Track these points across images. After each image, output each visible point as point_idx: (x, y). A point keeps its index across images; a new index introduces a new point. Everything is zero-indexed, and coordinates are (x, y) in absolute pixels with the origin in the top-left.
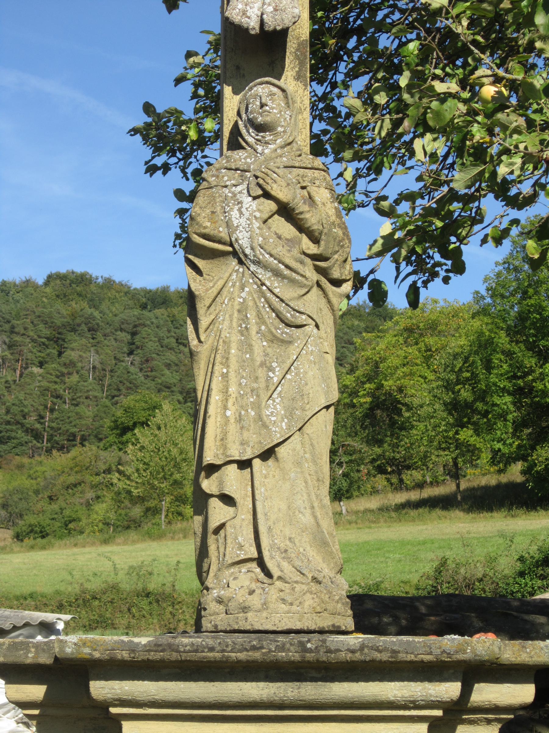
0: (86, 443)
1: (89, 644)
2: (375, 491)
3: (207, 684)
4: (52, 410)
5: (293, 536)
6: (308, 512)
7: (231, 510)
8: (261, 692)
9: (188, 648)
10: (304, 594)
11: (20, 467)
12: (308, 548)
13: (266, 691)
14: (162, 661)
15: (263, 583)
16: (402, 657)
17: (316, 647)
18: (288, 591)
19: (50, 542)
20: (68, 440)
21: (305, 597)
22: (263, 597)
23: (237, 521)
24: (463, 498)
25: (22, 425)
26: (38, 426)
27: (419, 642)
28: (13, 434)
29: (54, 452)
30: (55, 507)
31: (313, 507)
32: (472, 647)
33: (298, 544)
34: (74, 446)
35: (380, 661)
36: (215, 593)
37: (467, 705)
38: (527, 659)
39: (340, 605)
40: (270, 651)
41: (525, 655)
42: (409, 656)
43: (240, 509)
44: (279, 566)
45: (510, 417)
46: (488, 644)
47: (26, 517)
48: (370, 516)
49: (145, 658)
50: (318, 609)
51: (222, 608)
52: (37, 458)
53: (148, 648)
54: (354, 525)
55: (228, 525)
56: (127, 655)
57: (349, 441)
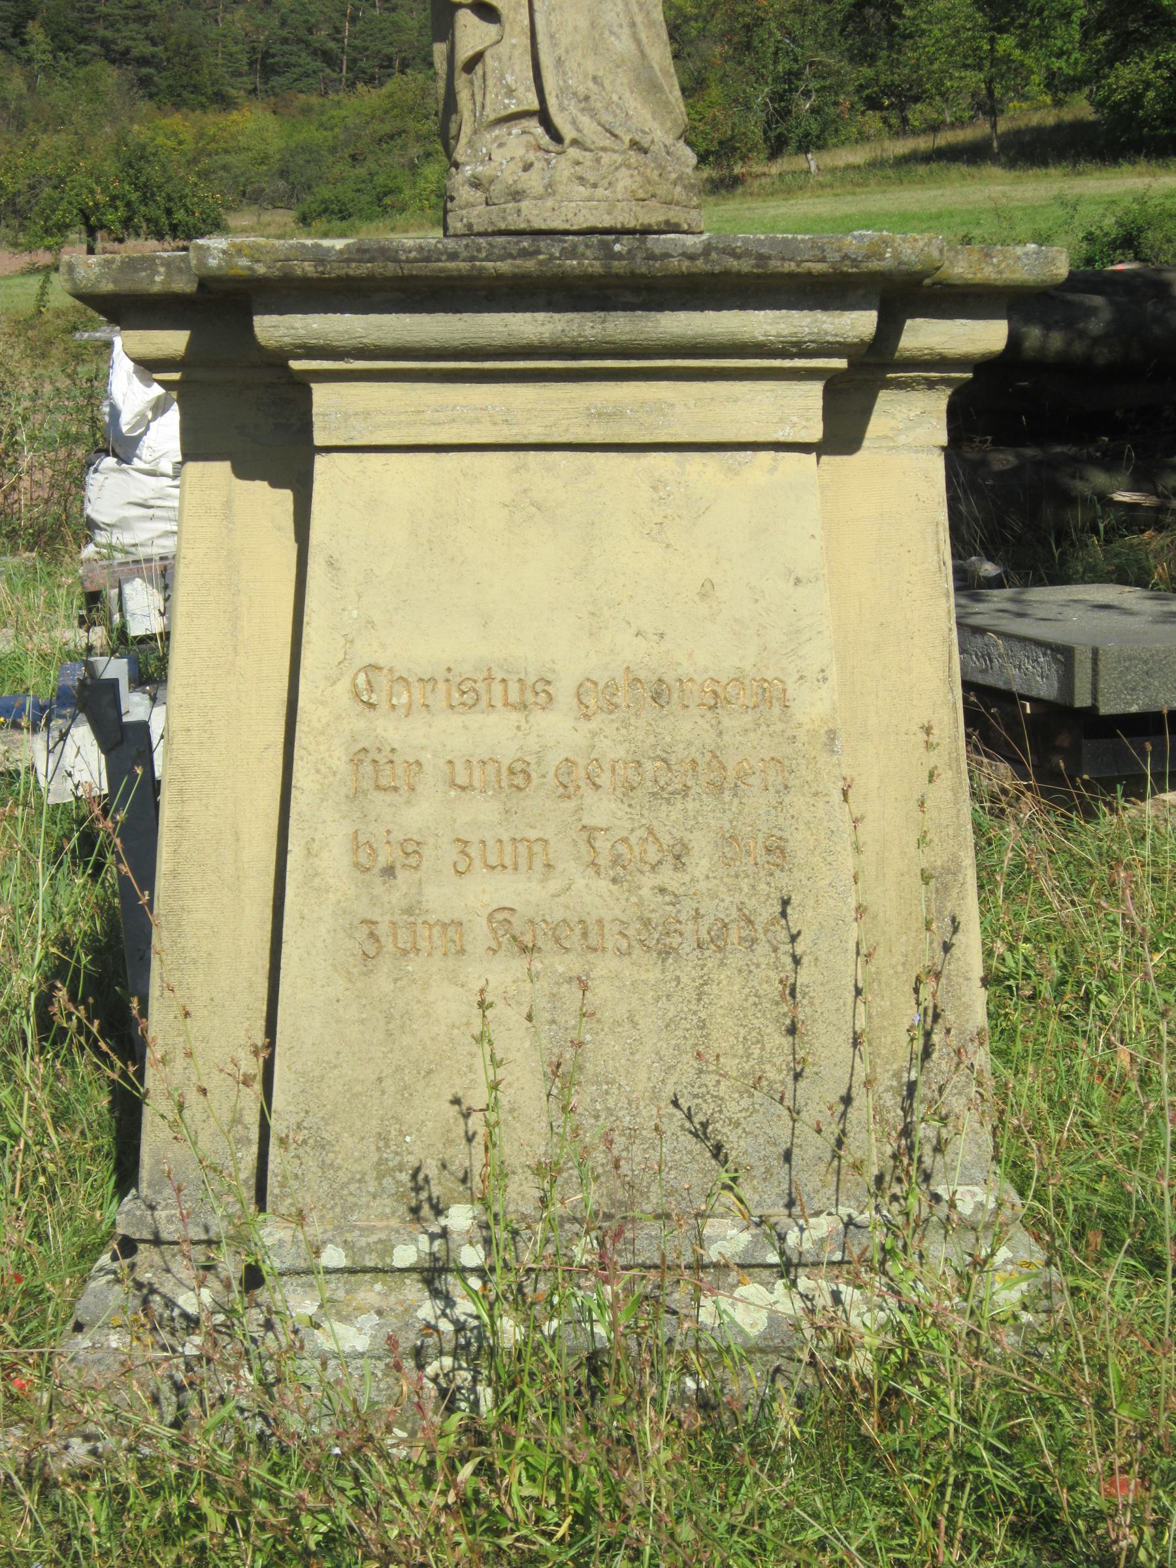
0: (408, 71)
1: (246, 251)
2: (863, 138)
3: (450, 317)
4: (354, 20)
5: (600, 73)
6: (625, 32)
7: (492, 29)
8: (540, 329)
9: (413, 254)
10: (617, 169)
11: (306, 111)
12: (627, 95)
13: (549, 327)
14: (371, 278)
15: (548, 152)
16: (775, 265)
17: (629, 251)
18: (588, 163)
19: (353, 225)
20: (381, 67)
21: (618, 175)
22: (547, 175)
23: (503, 49)
24: (1002, 146)
25: (308, 44)
26: (332, 45)
27: (803, 241)
28: (294, 59)
29: (359, 85)
30: (361, 171)
31: (633, 25)
32: (895, 249)
33: (608, 87)
34: (389, 76)
35: (739, 274)
36: (468, 170)
37: (893, 353)
38: (993, 276)
39: (678, 189)
40: (552, 257)
41: (990, 269)
42: (786, 264)
43: (507, 26)
44: (574, 122)
45: (1076, 16)
46: (921, 244)
47: (315, 190)
48: (851, 175)
49: (343, 272)
50: (641, 194)
51: (479, 195)
52: (332, 96)
53: (346, 257)
54: (828, 190)
55: (487, 55)
56: (311, 269)
57: (821, 56)
